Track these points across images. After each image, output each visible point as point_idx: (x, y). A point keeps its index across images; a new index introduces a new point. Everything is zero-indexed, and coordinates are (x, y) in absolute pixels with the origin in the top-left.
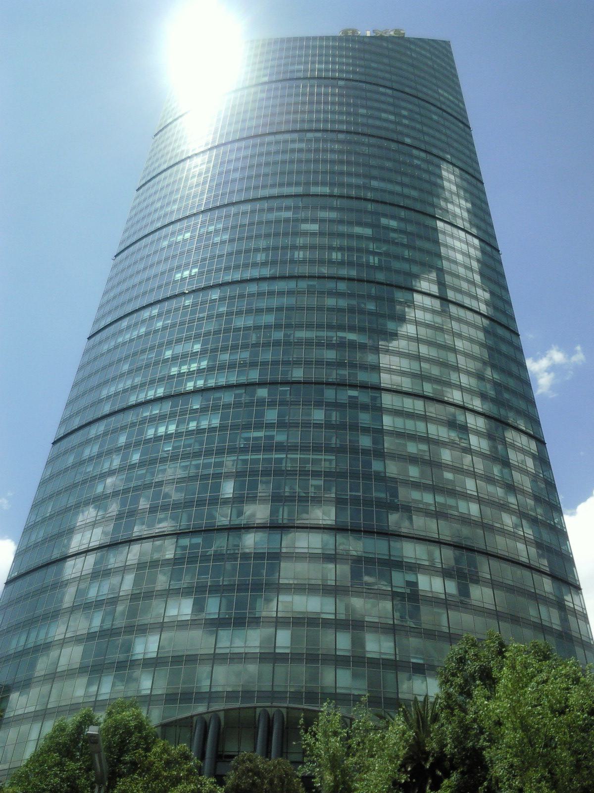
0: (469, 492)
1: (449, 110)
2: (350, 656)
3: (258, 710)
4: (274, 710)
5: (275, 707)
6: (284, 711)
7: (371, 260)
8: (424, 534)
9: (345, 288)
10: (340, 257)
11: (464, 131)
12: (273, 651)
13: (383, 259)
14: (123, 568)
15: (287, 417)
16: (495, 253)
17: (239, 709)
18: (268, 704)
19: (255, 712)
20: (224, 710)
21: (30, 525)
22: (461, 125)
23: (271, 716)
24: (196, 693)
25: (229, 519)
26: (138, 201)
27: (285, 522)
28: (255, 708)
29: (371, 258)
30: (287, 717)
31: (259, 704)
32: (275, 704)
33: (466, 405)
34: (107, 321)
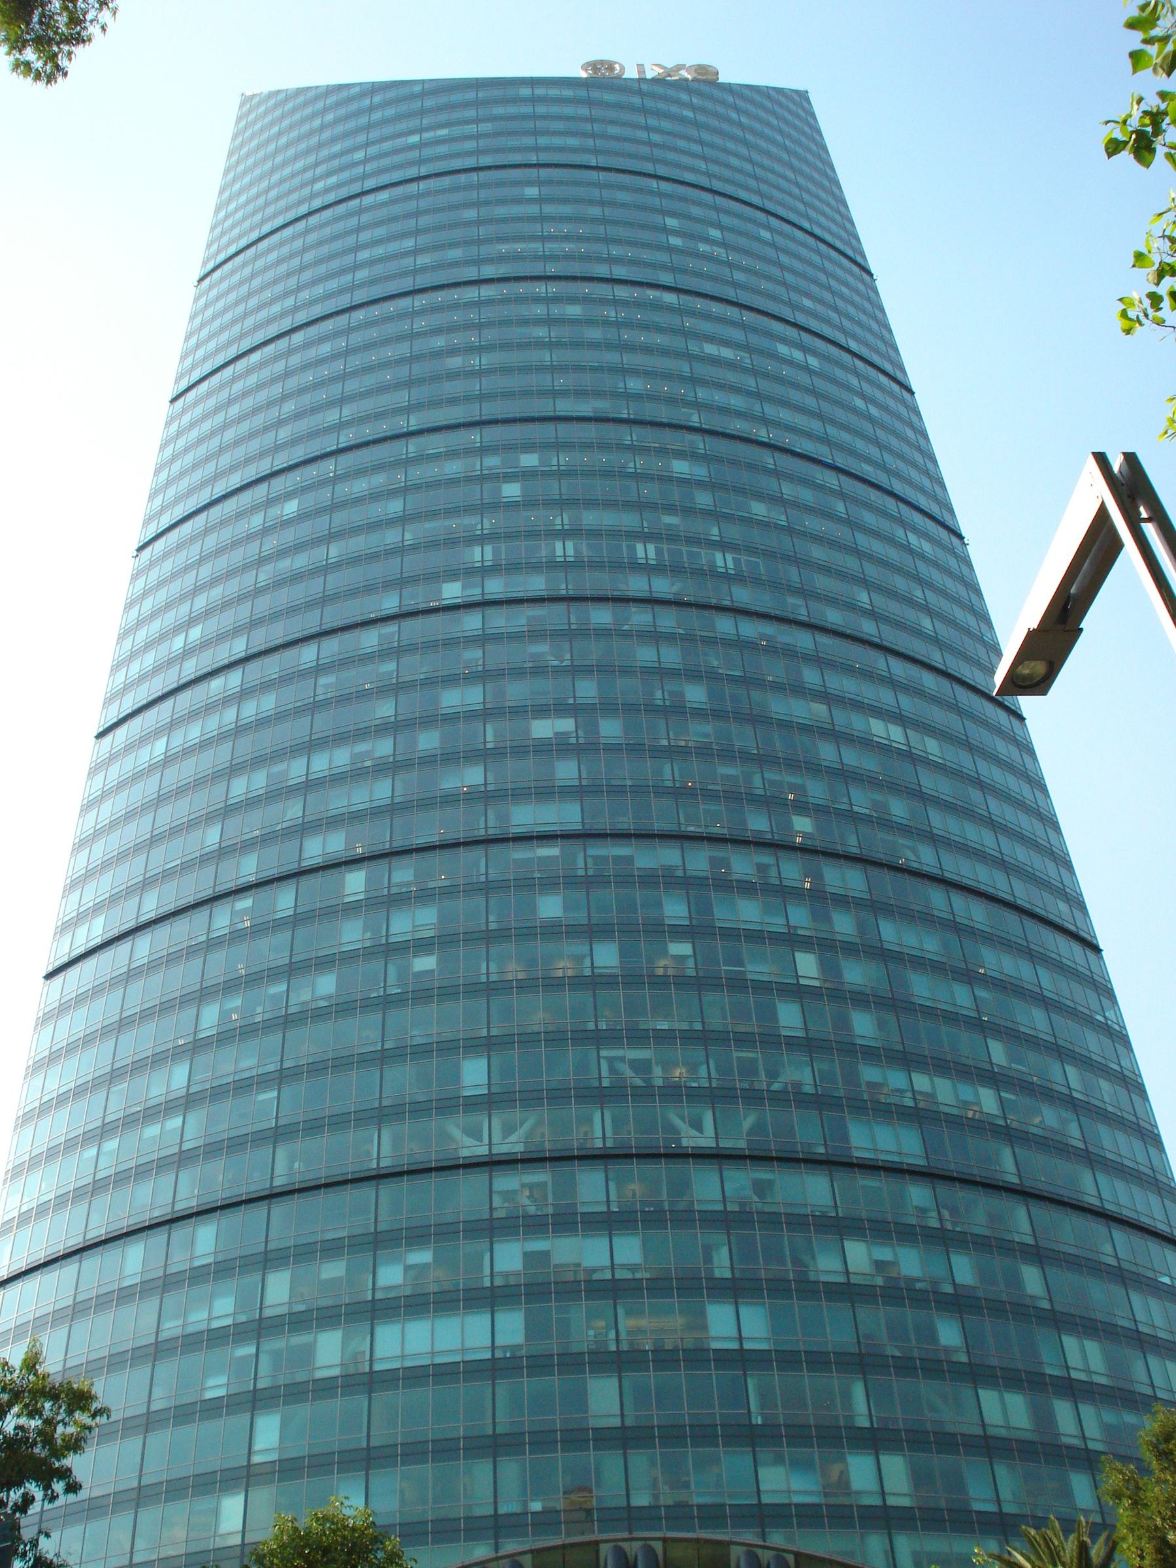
0: (936, 913)
1: (828, 238)
2: (770, 1351)
3: (605, 1549)
4: (637, 1545)
5: (637, 1539)
6: (658, 1547)
7: (719, 562)
8: (896, 1159)
9: (673, 624)
10: (652, 554)
11: (863, 281)
12: (605, 1210)
13: (744, 558)
14: (277, 1075)
15: (564, 586)
16: (906, 395)
17: (564, 1546)
18: (626, 1535)
19: (597, 1552)
20: (531, 1551)
21: (66, 919)
22: (855, 269)
23: (631, 1559)
24: (464, 1438)
25: (486, 1141)
26: (189, 361)
27: (609, 1144)
28: (597, 1543)
29: (719, 556)
30: (665, 1560)
31: (605, 1536)
32: (636, 1534)
33: (946, 874)
34: (174, 515)
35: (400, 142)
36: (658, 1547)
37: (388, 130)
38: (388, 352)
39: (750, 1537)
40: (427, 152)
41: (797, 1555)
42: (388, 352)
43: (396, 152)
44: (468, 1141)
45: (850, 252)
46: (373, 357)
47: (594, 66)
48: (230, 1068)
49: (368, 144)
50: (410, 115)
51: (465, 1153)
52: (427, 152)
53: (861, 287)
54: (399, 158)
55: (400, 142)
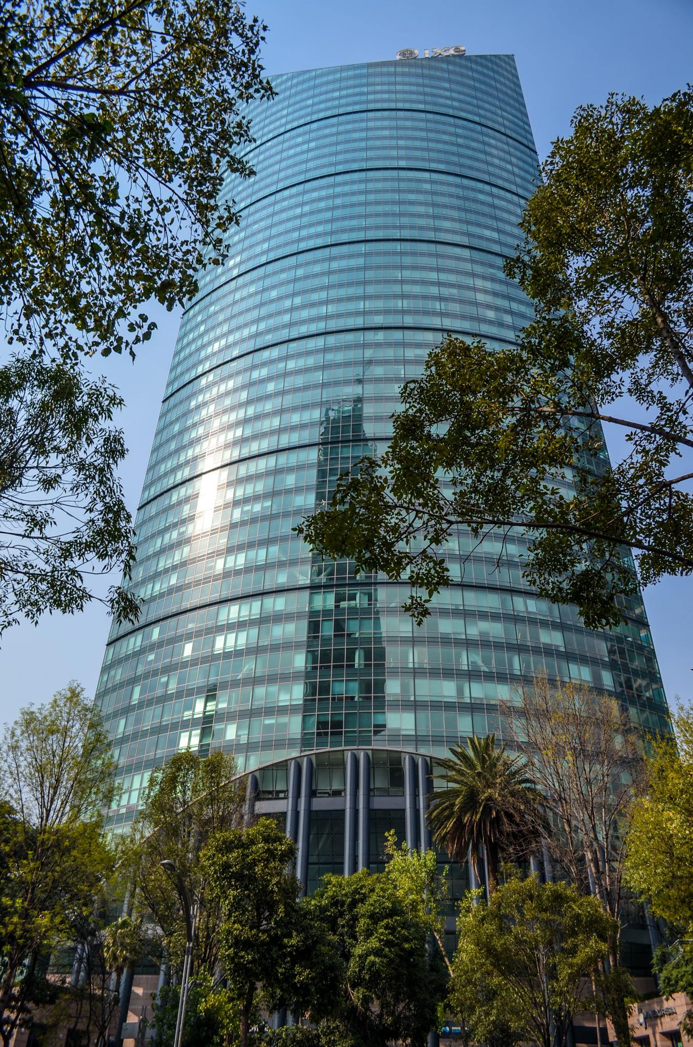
6: (370, 753)
11: (530, 157)
35: (329, 96)
36: (370, 753)
37: (351, 83)
38: (320, 229)
39: (411, 749)
40: (315, 108)
41: (431, 758)
42: (320, 229)
43: (301, 109)
44: (301, 577)
45: (526, 142)
46: (312, 230)
47: (403, 54)
48: (213, 708)
49: (289, 106)
50: (309, 89)
51: (301, 583)
52: (315, 108)
53: (529, 160)
54: (303, 112)
55: (329, 96)
